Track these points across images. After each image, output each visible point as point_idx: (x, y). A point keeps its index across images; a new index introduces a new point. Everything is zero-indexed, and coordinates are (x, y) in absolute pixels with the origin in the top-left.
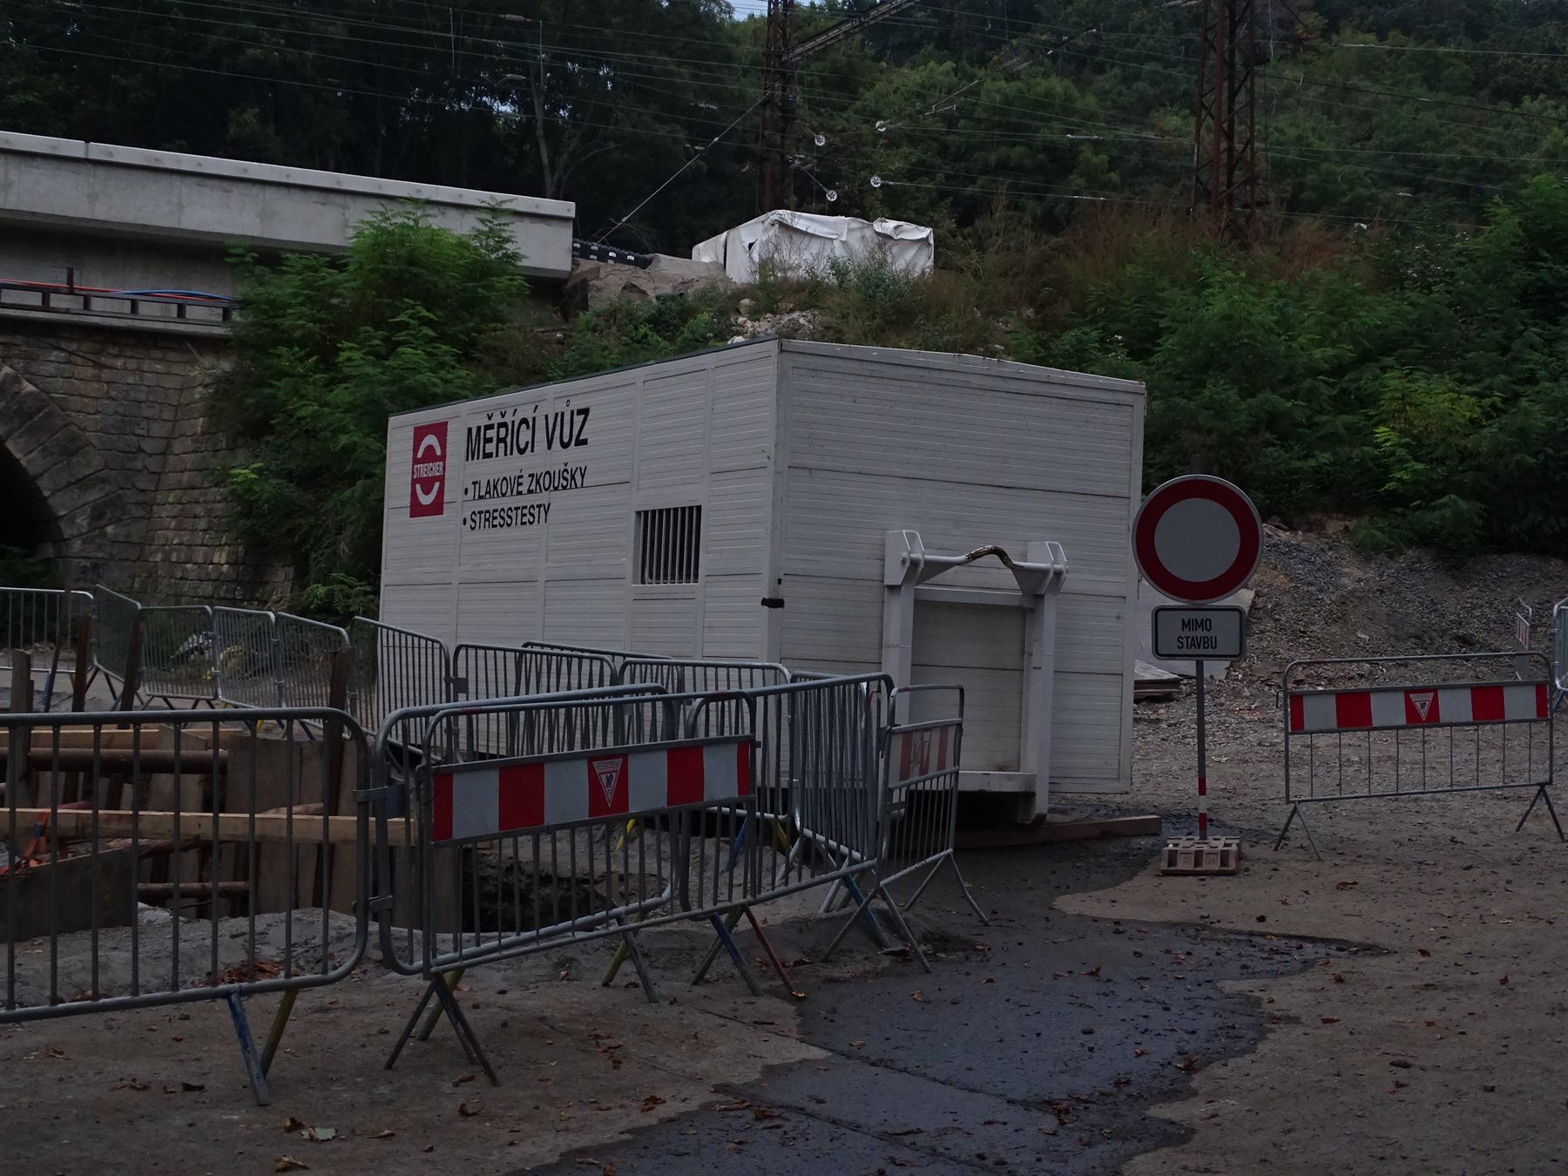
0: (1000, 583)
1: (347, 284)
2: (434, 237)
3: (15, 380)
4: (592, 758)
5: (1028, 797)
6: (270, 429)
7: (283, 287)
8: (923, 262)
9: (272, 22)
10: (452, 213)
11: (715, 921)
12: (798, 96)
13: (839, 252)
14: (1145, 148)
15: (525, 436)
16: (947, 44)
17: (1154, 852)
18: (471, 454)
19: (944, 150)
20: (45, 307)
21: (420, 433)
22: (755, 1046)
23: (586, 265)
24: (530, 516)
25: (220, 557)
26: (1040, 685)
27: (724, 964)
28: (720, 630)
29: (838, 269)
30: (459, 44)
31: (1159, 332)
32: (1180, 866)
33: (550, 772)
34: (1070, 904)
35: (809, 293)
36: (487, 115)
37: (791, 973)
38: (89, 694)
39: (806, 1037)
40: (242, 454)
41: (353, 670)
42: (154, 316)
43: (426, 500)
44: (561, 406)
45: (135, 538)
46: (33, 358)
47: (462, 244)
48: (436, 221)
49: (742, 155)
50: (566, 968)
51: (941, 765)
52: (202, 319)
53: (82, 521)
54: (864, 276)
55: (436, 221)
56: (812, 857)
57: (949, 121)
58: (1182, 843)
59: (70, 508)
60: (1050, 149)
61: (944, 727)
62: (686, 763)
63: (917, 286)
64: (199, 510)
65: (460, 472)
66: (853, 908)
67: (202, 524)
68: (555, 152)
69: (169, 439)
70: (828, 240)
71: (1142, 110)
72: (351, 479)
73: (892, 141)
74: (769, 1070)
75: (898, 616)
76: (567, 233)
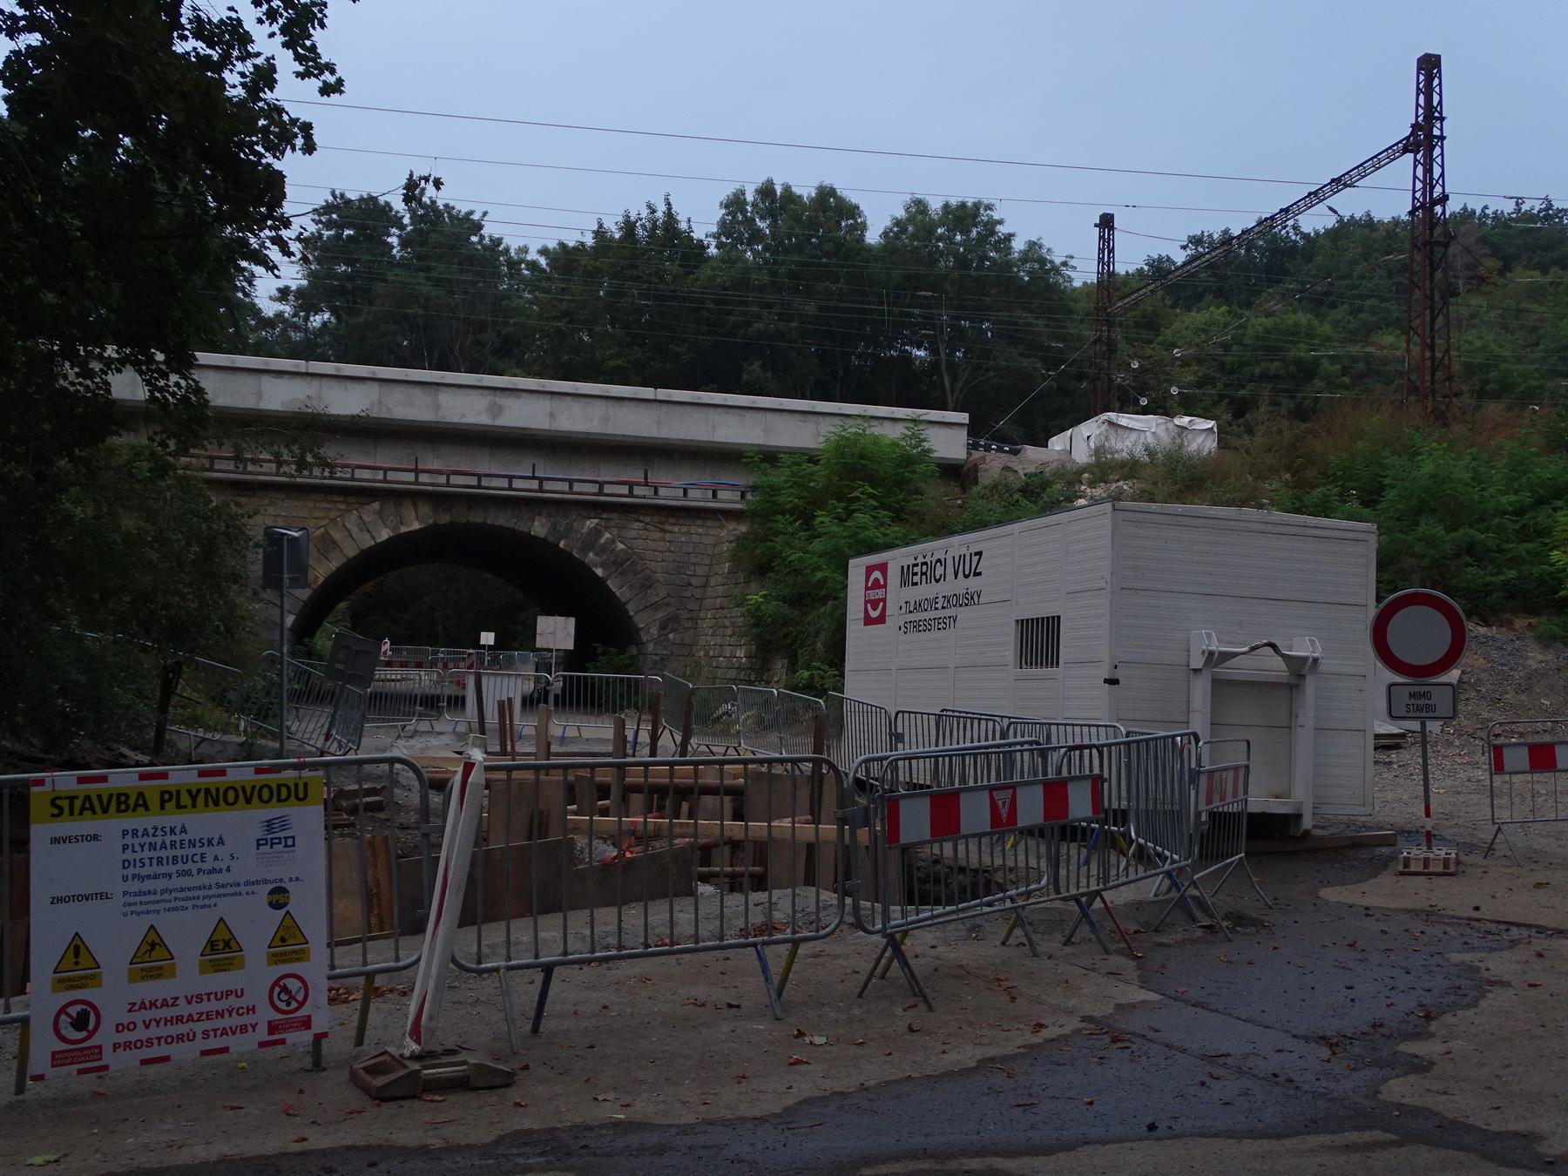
0: (1274, 667)
2: (876, 440)
3: (613, 541)
4: (992, 789)
5: (1298, 817)
6: (771, 569)
7: (779, 477)
8: (1210, 445)
9: (770, 306)
10: (887, 424)
12: (1118, 334)
13: (1150, 439)
14: (1368, 359)
15: (939, 571)
16: (1222, 295)
18: (904, 583)
19: (1222, 366)
20: (631, 494)
23: (976, 455)
24: (943, 624)
25: (740, 653)
26: (1304, 740)
27: (1084, 931)
29: (1151, 452)
31: (1383, 488)
32: (1412, 869)
34: (1331, 894)
35: (1130, 468)
37: (1132, 939)
38: (660, 743)
39: (1145, 984)
40: (754, 586)
41: (828, 727)
42: (697, 498)
43: (874, 614)
44: (963, 551)
45: (687, 641)
46: (622, 527)
47: (895, 444)
49: (1081, 377)
50: (975, 932)
51: (1235, 794)
52: (728, 499)
53: (654, 631)
55: (877, 430)
57: (1226, 347)
58: (1416, 852)
59: (646, 622)
60: (1298, 362)
61: (1236, 768)
62: (1056, 792)
63: (1206, 461)
64: (727, 623)
65: (896, 595)
66: (1174, 894)
67: (729, 632)
68: (954, 380)
69: (707, 577)
70: (1142, 432)
72: (824, 600)
73: (1185, 362)
74: (1119, 1007)
75: (1200, 691)
76: (964, 433)
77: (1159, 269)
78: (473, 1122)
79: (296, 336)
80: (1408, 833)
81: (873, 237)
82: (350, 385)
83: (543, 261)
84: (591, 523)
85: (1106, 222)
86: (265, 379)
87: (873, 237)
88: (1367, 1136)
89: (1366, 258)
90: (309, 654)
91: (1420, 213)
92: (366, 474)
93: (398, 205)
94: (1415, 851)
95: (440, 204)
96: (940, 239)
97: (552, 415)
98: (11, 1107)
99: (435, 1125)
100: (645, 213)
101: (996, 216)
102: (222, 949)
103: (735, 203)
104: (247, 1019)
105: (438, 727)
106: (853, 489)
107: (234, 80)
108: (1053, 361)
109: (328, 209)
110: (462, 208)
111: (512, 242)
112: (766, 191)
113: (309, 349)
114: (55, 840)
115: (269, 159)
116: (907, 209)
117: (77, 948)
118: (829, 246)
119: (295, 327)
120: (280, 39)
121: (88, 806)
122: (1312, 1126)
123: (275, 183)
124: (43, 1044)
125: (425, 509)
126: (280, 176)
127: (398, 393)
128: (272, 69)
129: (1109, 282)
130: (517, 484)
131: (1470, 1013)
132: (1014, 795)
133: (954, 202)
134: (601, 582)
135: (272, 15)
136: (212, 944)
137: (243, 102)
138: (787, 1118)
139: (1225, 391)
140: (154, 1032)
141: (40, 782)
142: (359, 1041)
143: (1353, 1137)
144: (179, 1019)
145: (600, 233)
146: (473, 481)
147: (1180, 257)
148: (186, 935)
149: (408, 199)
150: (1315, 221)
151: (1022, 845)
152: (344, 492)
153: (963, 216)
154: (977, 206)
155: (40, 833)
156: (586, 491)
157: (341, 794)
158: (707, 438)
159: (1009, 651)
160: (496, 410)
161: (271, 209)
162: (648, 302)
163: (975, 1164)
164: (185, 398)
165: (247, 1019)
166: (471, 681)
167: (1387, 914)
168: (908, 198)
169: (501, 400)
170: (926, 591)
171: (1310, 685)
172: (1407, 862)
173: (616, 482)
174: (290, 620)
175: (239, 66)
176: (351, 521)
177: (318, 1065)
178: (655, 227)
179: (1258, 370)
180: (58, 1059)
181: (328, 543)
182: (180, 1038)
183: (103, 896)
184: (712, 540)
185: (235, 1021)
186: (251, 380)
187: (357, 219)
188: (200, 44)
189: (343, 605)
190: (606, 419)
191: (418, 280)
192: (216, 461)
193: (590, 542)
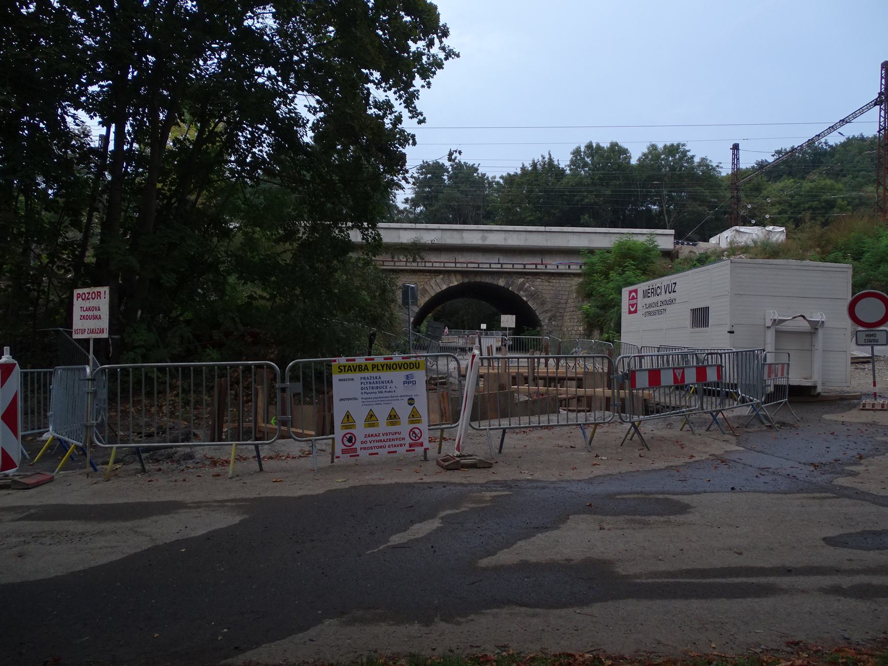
0: (804, 325)
1: (611, 258)
2: (635, 243)
4: (674, 369)
5: (815, 387)
6: (592, 295)
7: (595, 259)
8: (783, 237)
9: (592, 192)
10: (639, 236)
11: (712, 414)
12: (742, 194)
13: (755, 237)
14: (860, 198)
15: (659, 291)
16: (791, 174)
17: (859, 404)
18: (644, 297)
19: (790, 205)
21: (630, 292)
22: (719, 445)
23: (678, 247)
24: (660, 312)
25: (581, 328)
26: (818, 357)
27: (715, 426)
28: (715, 339)
29: (755, 242)
30: (641, 191)
31: (863, 252)
32: (867, 407)
33: (662, 372)
34: (827, 417)
35: (745, 249)
36: (650, 210)
37: (736, 430)
39: (738, 444)
40: (585, 302)
42: (563, 269)
43: (632, 310)
44: (668, 283)
47: (642, 244)
48: (635, 238)
49: (725, 213)
50: (670, 425)
51: (782, 374)
52: (575, 269)
53: (546, 321)
54: (763, 243)
55: (635, 238)
56: (743, 401)
57: (792, 197)
58: (869, 401)
60: (826, 201)
61: (783, 364)
62: (701, 372)
63: (780, 245)
65: (641, 302)
66: (755, 413)
68: (669, 218)
70: (751, 233)
71: (859, 187)
72: (614, 307)
73: (773, 204)
74: (726, 452)
75: (770, 335)
76: (673, 238)
77: (762, 166)
78: (478, 477)
79: (411, 216)
80: (867, 395)
81: (634, 161)
82: (431, 232)
83: (501, 181)
84: (521, 280)
85: (736, 147)
86: (401, 231)
87: (634, 161)
88: (823, 495)
89: (860, 153)
90: (419, 332)
91: (882, 132)
92: (437, 265)
93: (447, 164)
94: (868, 401)
95: (462, 162)
96: (663, 160)
97: (505, 239)
98: (330, 467)
99: (465, 477)
100: (540, 159)
101: (687, 148)
102: (393, 418)
103: (577, 152)
104: (402, 442)
105: (466, 357)
106: (625, 262)
107: (388, 122)
108: (712, 207)
109: (422, 167)
110: (470, 163)
111: (490, 175)
112: (589, 146)
113: (416, 220)
114: (340, 380)
115: (401, 149)
116: (648, 149)
117: (348, 416)
118: (616, 166)
119: (411, 213)
120: (403, 105)
121: (350, 369)
122: (801, 491)
123: (403, 157)
124: (339, 447)
125: (459, 277)
126: (405, 155)
127: (448, 234)
128: (401, 116)
129: (737, 173)
130: (493, 266)
131: (880, 458)
132: (683, 373)
133: (668, 144)
134: (526, 302)
135: (400, 97)
136: (390, 416)
137: (391, 130)
138: (590, 481)
139: (790, 216)
140: (373, 444)
141: (335, 361)
142: (439, 453)
143: (818, 495)
144: (381, 441)
145: (523, 168)
146: (476, 265)
147: (771, 160)
148: (383, 414)
149: (450, 160)
150: (834, 139)
151: (693, 398)
152: (429, 271)
153: (672, 150)
154: (678, 145)
155: (336, 377)
156: (519, 268)
157: (431, 378)
158: (566, 245)
159: (688, 322)
160: (484, 238)
161: (402, 167)
162: (544, 194)
163: (661, 496)
164: (374, 238)
165: (402, 442)
166: (477, 340)
167: (851, 424)
168: (648, 144)
169: (486, 234)
170: (654, 299)
171: (820, 332)
172: (864, 405)
173: (530, 263)
174: (412, 319)
175: (390, 117)
176: (432, 282)
177: (426, 459)
178: (545, 164)
179: (807, 206)
180: (344, 452)
181: (425, 291)
182: (381, 447)
183: (356, 399)
184: (568, 285)
185: (398, 442)
186: (395, 232)
187: (433, 170)
188: (376, 110)
189: (430, 315)
190: (526, 239)
191: (456, 192)
192: (385, 262)
193: (521, 287)
